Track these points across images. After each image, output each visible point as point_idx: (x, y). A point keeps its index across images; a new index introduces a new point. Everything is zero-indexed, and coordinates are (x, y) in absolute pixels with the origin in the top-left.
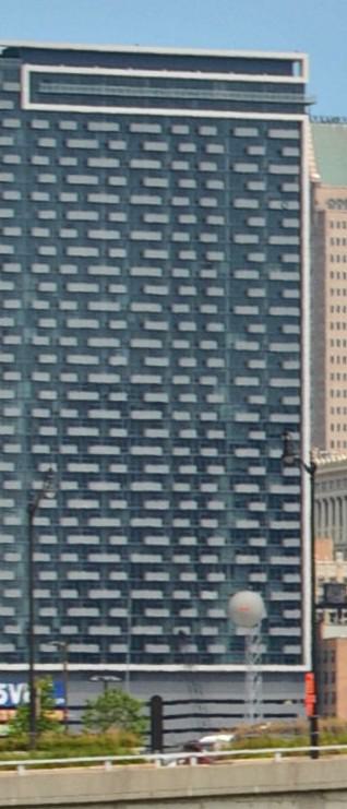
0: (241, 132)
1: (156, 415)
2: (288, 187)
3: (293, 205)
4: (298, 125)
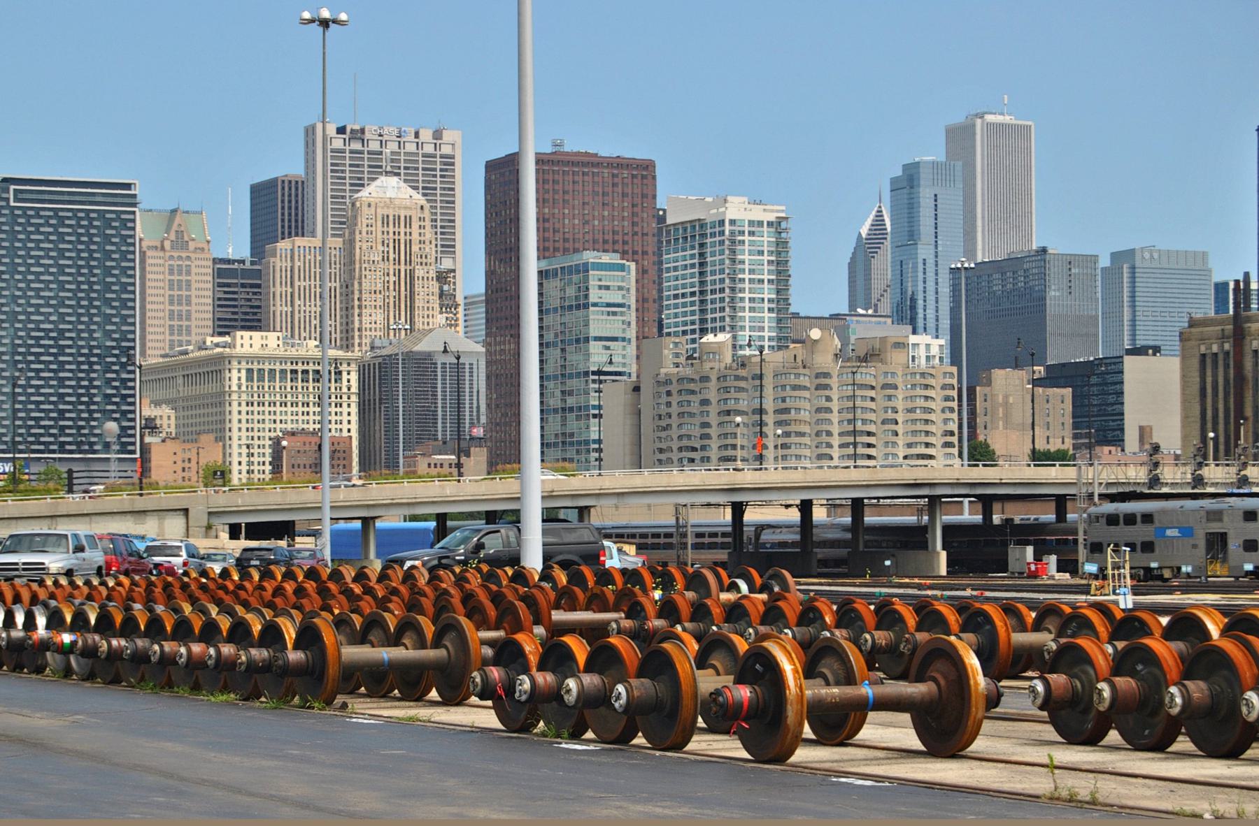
0: (108, 216)
3: (131, 249)
4: (134, 213)
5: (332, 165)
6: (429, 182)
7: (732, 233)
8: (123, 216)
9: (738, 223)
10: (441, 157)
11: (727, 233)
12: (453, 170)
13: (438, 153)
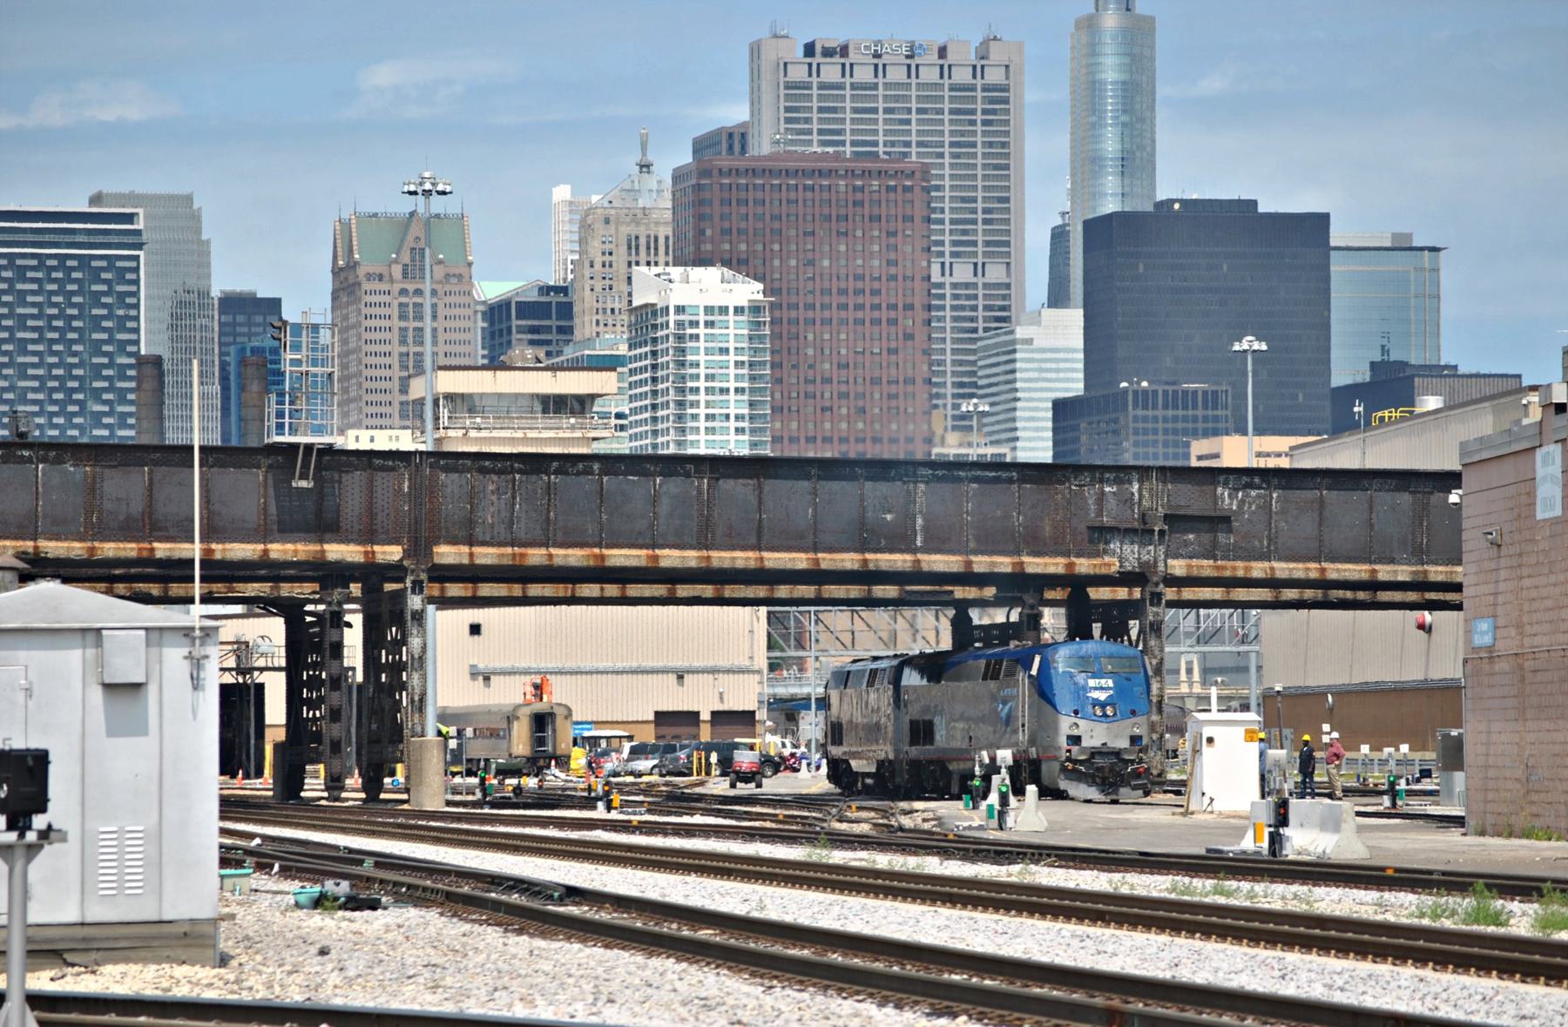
0: (94, 264)
1: (36, 360)
2: (129, 300)
3: (133, 313)
4: (137, 258)
5: (787, 110)
6: (962, 134)
7: (680, 324)
8: (119, 264)
9: (688, 310)
10: (985, 89)
11: (672, 324)
12: (1007, 111)
13: (979, 82)
